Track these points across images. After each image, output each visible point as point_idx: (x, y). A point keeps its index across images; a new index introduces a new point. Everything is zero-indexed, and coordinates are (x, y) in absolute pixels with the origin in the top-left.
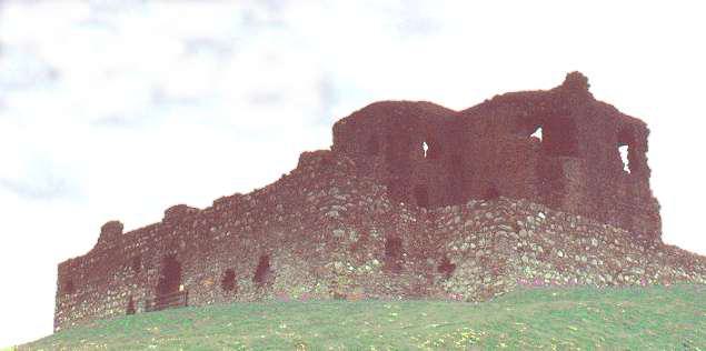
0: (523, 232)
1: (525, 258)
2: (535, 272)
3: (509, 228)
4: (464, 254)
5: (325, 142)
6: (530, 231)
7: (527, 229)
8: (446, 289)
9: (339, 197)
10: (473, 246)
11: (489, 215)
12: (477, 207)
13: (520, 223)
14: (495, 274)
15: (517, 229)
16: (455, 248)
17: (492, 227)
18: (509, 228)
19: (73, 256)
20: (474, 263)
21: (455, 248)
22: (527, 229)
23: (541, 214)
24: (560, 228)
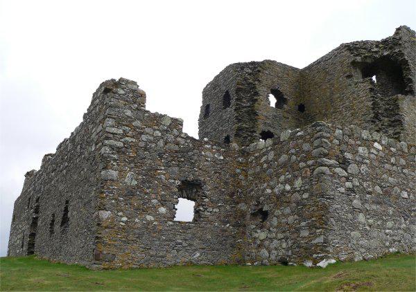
0: (353, 168)
1: (356, 203)
2: (371, 221)
3: (332, 162)
4: (278, 198)
5: (86, 112)
6: (363, 167)
7: (359, 163)
8: (259, 242)
9: (114, 130)
10: (288, 187)
11: (306, 147)
12: (293, 137)
13: (348, 156)
14: (311, 227)
15: (344, 163)
16: (269, 191)
17: (310, 162)
18: (332, 162)
19: (243, 60)
20: (288, 211)
21: (269, 191)
22: (359, 163)
23: (376, 145)
24: (403, 162)
